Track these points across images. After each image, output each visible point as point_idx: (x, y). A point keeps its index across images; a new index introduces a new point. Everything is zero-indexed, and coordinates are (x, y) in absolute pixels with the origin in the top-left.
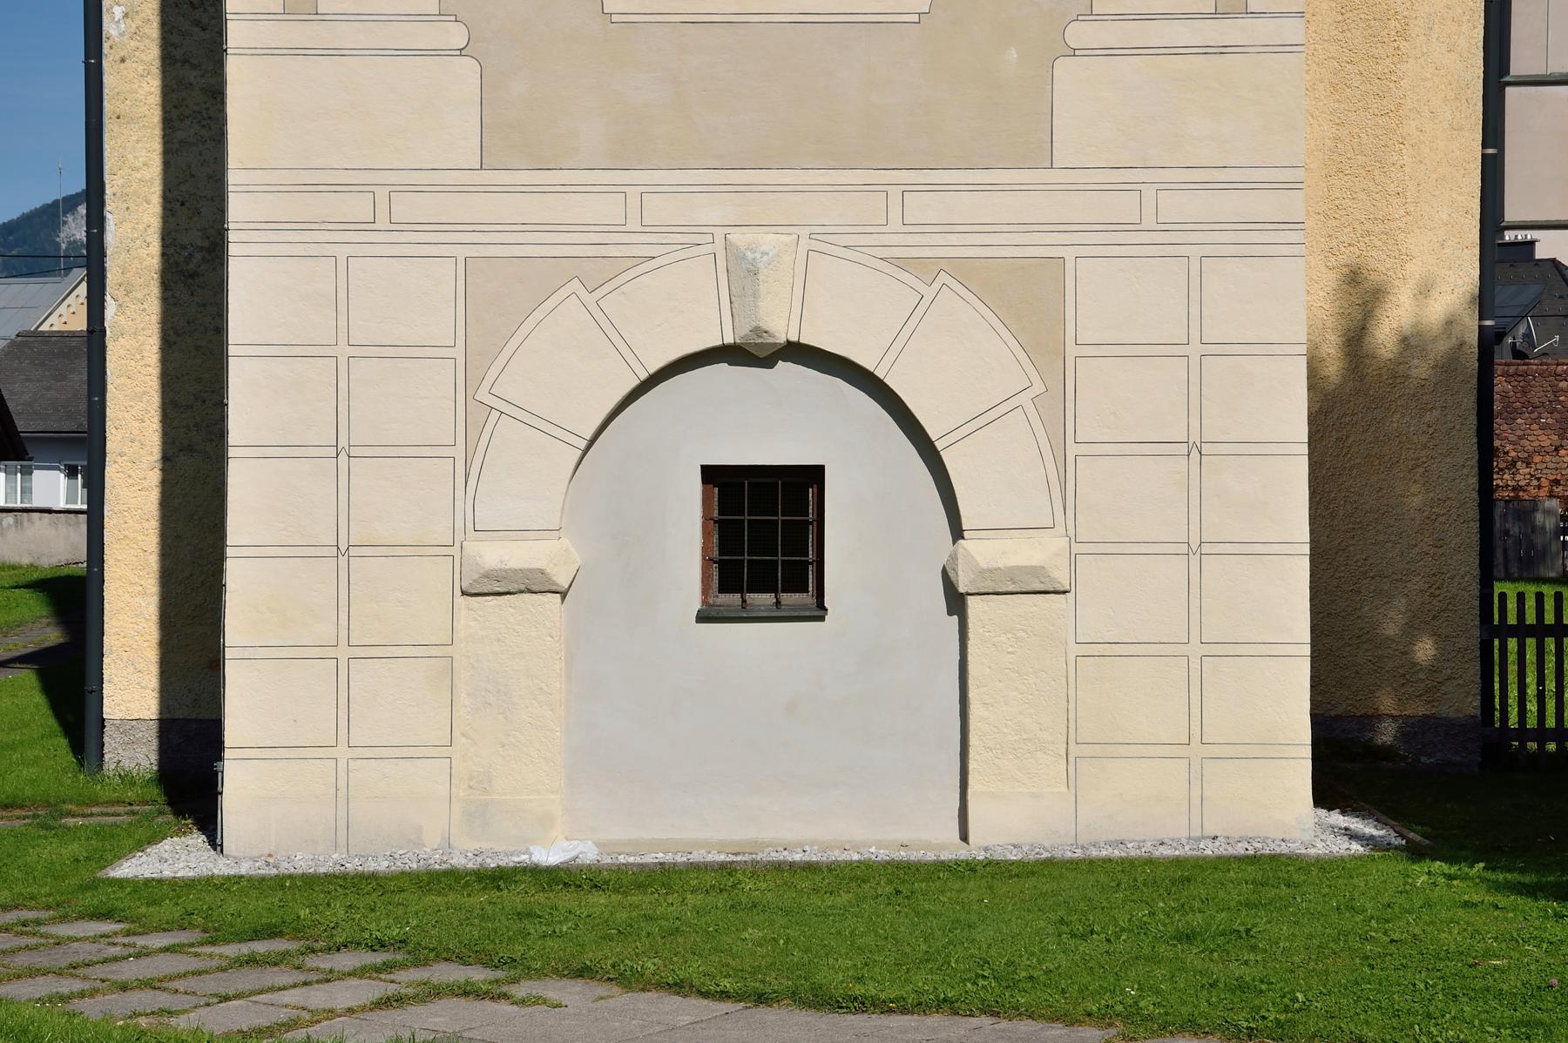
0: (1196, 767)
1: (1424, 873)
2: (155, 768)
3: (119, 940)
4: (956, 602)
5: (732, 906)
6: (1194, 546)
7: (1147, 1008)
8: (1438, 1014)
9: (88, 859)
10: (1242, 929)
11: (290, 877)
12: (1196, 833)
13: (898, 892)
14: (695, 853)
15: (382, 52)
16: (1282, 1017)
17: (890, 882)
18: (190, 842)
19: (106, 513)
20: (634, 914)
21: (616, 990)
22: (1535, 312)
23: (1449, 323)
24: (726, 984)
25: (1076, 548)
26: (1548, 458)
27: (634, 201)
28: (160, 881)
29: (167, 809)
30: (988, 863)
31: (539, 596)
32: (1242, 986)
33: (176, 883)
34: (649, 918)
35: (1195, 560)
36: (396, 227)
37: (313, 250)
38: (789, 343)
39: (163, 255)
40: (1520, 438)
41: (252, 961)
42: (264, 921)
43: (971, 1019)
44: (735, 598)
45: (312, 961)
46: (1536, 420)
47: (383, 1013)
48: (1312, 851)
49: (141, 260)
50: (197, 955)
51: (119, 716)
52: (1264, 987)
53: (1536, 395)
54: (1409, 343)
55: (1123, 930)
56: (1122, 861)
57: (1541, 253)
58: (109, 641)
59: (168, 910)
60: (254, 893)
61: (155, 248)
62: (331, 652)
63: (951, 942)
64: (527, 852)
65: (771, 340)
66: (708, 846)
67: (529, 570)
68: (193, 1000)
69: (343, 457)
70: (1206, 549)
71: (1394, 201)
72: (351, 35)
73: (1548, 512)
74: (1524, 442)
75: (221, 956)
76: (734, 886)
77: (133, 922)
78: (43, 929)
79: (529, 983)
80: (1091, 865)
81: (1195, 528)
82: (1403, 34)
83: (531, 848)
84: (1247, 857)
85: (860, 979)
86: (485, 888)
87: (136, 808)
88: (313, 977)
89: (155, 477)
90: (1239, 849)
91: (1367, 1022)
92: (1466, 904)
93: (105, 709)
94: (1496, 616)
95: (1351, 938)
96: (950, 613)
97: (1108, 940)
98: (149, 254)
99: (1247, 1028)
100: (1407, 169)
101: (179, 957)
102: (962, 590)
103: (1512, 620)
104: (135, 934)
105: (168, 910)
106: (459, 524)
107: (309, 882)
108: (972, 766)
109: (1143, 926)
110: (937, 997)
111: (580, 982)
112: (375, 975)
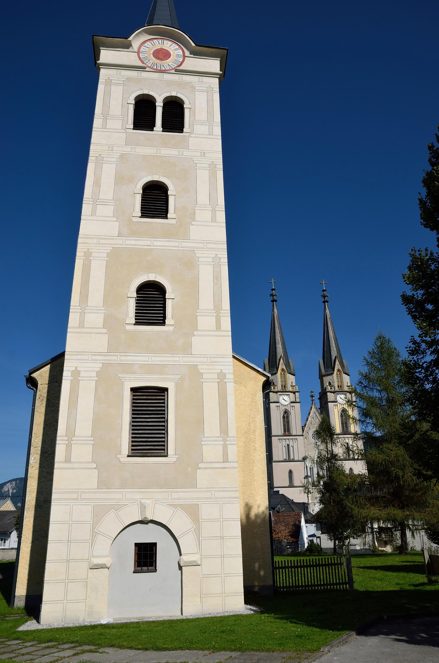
0: (223, 598)
1: (264, 617)
2: (24, 606)
3: (21, 644)
4: (180, 568)
5: (140, 631)
6: (222, 556)
7: (216, 646)
8: (266, 643)
9: (13, 627)
10: (232, 629)
11: (54, 628)
12: (224, 611)
13: (170, 626)
14: (132, 620)
15: (81, 468)
16: (240, 646)
17: (169, 624)
18: (33, 622)
19: (20, 553)
20: (121, 633)
21: (119, 649)
22: (280, 504)
23: (263, 512)
24: (140, 647)
25: (202, 557)
26: (284, 531)
27: (124, 495)
28: (28, 631)
29: (27, 615)
30: (187, 619)
31: (104, 569)
32: (233, 641)
33: (31, 631)
34: (124, 634)
35: (222, 558)
36: (82, 499)
37: (67, 504)
38: (151, 520)
39: (36, 502)
40: (279, 528)
41: (48, 647)
42: (50, 638)
43: (186, 651)
44: (140, 568)
45: (60, 647)
46: (281, 524)
47: (75, 657)
48: (244, 613)
49: (32, 503)
50: (37, 647)
51: (18, 595)
52: (236, 641)
53: (281, 520)
54: (256, 516)
55: (212, 631)
56: (211, 617)
57: (280, 493)
58: (18, 579)
59: (30, 637)
60: (47, 632)
61: (34, 501)
62: (64, 581)
63: (181, 636)
64: (100, 621)
65: (148, 519)
66: (134, 618)
67: (103, 564)
68: (37, 657)
69: (69, 542)
70: (224, 556)
71: (254, 491)
72: (76, 465)
73: (284, 542)
74: (279, 529)
75: (42, 646)
76: (139, 626)
77: (23, 640)
78: (5, 643)
79: (102, 649)
80: (205, 618)
81: (222, 552)
82: (254, 462)
83: (101, 620)
84: (233, 615)
85: (164, 644)
86: (91, 629)
87: (20, 615)
88: (60, 650)
89: (30, 545)
90: (232, 614)
91: (254, 646)
92: (271, 622)
93: (16, 593)
94: (275, 566)
95: (251, 630)
96: (179, 570)
97: (209, 633)
98: (33, 502)
99: (234, 649)
100: (256, 485)
101: (33, 647)
102: (181, 565)
103: (277, 566)
104: (24, 643)
105: (30, 637)
106: (90, 555)
107: (58, 629)
108: (183, 600)
109: (215, 630)
110: (179, 647)
111: (112, 648)
112: (72, 649)
